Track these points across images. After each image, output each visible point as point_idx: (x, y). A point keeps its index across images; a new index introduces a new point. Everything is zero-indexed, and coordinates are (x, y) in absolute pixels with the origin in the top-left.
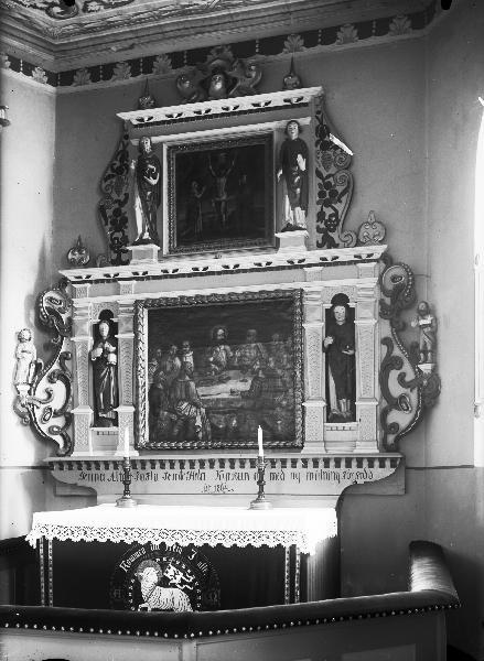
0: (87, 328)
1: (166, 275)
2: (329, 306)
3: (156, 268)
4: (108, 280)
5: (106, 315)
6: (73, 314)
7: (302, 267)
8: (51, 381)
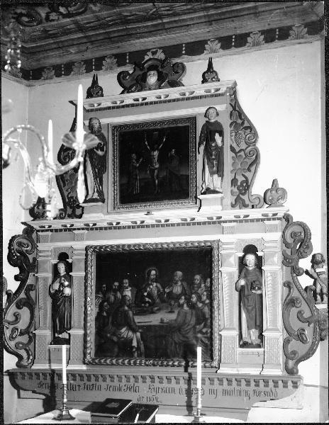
2: (241, 254)
8: (18, 307)
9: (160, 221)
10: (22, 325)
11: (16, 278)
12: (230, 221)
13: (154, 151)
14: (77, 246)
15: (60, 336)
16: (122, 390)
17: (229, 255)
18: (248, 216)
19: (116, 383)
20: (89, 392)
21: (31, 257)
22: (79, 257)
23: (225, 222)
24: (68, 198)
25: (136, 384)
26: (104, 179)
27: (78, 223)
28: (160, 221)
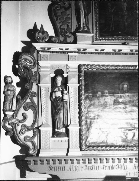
0: (49, 80)
1: (97, 53)
2: (53, 75)
3: (91, 48)
4: (61, 52)
5: (59, 72)
6: (38, 69)
7: (68, 52)
8: (25, 109)
9: (80, 50)
10: (29, 122)
11: (18, 85)
12: (74, 52)
13: (124, 2)
14: (71, 66)
15: (59, 131)
16: (115, 168)
17: (45, 76)
18: (103, 50)
19: (110, 163)
20: (90, 171)
21: (34, 70)
22: (73, 73)
23: (71, 52)
24: (60, 29)
25: (125, 164)
26: (89, 18)
27: (72, 47)
28: (80, 50)
